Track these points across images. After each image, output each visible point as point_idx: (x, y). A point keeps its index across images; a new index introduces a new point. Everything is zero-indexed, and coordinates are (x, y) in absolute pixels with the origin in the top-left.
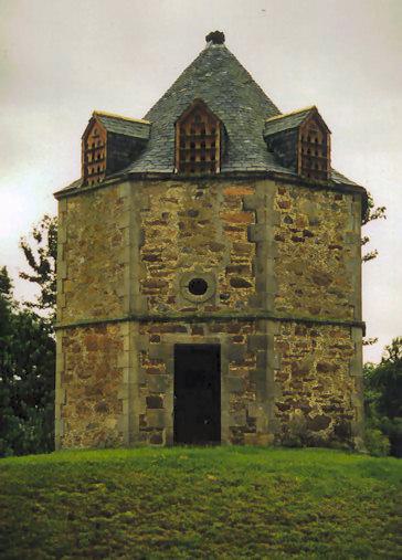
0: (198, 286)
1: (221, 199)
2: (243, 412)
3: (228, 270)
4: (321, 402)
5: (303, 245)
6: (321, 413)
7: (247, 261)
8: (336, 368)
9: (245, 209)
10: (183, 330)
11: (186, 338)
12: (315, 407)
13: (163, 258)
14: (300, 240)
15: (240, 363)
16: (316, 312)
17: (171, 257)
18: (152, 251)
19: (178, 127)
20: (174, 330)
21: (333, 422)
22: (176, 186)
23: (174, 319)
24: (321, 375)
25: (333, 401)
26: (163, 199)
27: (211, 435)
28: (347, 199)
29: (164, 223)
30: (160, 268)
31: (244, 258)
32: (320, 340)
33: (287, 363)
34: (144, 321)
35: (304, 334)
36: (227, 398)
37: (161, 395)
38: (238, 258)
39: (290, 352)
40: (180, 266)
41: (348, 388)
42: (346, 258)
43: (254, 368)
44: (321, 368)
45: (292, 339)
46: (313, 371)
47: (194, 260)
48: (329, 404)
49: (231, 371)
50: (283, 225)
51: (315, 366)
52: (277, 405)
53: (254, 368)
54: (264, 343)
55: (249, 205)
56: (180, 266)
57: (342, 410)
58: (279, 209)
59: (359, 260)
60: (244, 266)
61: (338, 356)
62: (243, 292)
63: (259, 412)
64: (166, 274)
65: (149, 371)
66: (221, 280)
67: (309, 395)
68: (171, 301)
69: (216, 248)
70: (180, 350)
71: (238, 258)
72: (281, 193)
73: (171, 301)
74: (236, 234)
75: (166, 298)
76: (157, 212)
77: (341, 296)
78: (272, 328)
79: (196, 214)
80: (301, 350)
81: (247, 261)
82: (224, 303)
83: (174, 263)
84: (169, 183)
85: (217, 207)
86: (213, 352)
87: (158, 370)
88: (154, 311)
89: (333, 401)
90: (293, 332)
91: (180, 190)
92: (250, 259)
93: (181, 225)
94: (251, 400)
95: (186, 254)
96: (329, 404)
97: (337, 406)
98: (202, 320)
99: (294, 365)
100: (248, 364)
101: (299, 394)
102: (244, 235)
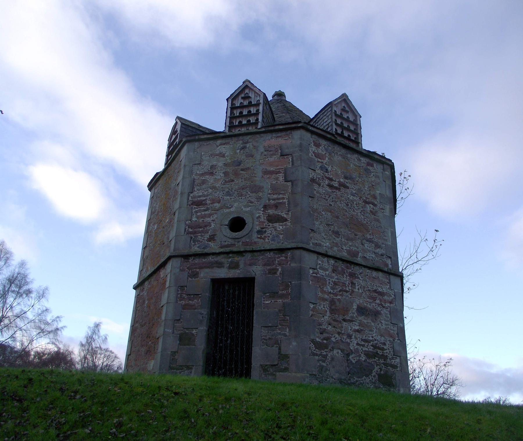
0: (237, 224)
1: (262, 149)
2: (275, 349)
3: (265, 207)
4: (363, 346)
5: (339, 193)
6: (363, 358)
7: (283, 198)
8: (376, 314)
9: (282, 155)
10: (220, 265)
11: (223, 273)
12: (357, 351)
13: (208, 202)
14: (336, 188)
15: (274, 295)
16: (356, 254)
17: (213, 201)
18: (200, 196)
19: (230, 102)
20: (211, 266)
21: (376, 368)
22: (224, 144)
23: (214, 254)
24: (361, 318)
25: (375, 347)
26: (213, 155)
27: (243, 370)
28: (378, 168)
29: (212, 174)
30: (205, 210)
31: (281, 196)
32: (360, 282)
33: (324, 300)
34: (186, 257)
35: (343, 273)
36: (259, 332)
37: (194, 331)
38: (275, 196)
39: (328, 288)
40: (221, 208)
41: (391, 336)
42: (380, 214)
43: (287, 301)
44: (362, 311)
45: (328, 276)
46: (353, 313)
47: (235, 202)
48: (371, 349)
49: (264, 305)
50: (319, 171)
51: (355, 307)
52: (313, 341)
53: (287, 301)
54: (300, 273)
55: (287, 151)
56: (221, 208)
57: (385, 358)
58: (314, 157)
59: (384, 157)
60: (281, 203)
61: (378, 301)
62: (279, 227)
63: (291, 347)
64: (210, 215)
65: (185, 307)
66: (259, 217)
67: (350, 336)
68: (212, 238)
69: (256, 189)
70: (217, 284)
71: (275, 196)
72: (317, 145)
73: (212, 238)
74: (273, 176)
75: (207, 236)
76: (207, 164)
77: (377, 246)
78: (309, 259)
79: (239, 163)
80: (339, 288)
81: (283, 198)
82: (260, 238)
83: (217, 205)
84: (219, 142)
85: (258, 156)
86: (248, 283)
87: (194, 305)
88: (196, 249)
89: (375, 347)
90: (330, 270)
91: (227, 146)
92: (286, 196)
93: (226, 174)
94: (285, 335)
95: (228, 197)
96: (371, 349)
97: (380, 352)
98: (239, 253)
99: (332, 302)
100: (282, 296)
101: (339, 333)
102: (281, 177)
